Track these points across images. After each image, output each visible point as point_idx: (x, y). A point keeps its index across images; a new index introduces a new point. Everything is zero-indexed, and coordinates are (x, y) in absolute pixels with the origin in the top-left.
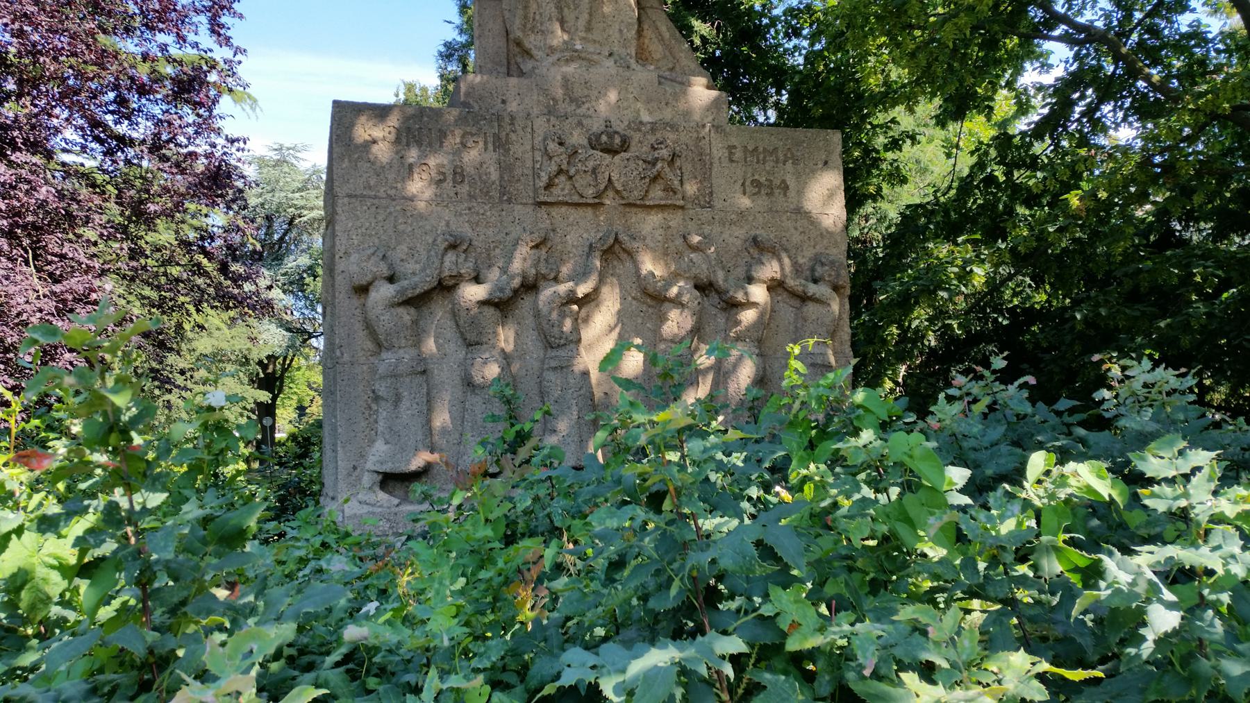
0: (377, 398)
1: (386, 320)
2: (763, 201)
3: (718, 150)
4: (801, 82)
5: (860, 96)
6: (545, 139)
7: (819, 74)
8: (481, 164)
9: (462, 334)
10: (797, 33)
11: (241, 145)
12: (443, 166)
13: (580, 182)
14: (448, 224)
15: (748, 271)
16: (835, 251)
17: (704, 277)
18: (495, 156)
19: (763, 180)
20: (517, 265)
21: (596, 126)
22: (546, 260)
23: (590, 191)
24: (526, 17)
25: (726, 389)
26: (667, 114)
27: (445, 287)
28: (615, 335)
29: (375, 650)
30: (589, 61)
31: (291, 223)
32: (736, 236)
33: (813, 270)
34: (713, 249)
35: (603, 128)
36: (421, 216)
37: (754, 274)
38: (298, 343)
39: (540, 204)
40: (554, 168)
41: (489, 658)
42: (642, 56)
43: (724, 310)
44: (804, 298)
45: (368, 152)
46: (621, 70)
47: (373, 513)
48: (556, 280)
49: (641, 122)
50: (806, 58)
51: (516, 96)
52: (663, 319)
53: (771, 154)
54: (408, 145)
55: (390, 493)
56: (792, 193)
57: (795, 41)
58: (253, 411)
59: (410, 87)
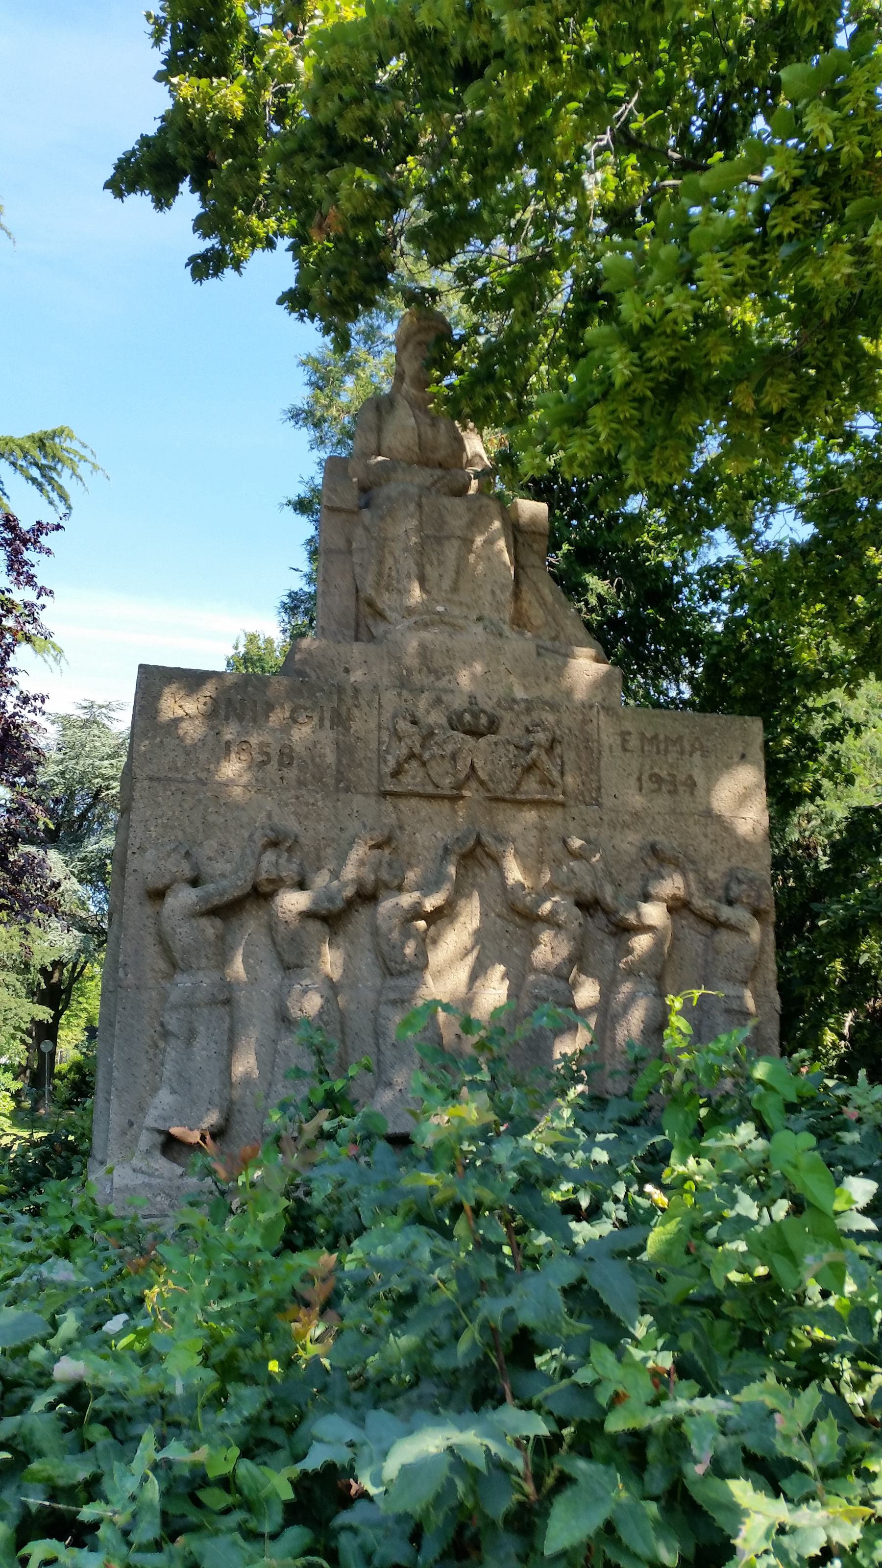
0: (166, 1034)
1: (184, 934)
2: (662, 802)
3: (607, 733)
4: (720, 654)
5: (792, 674)
6: (395, 716)
7: (742, 645)
8: (315, 743)
9: (279, 954)
10: (715, 596)
11: (38, 704)
12: (268, 745)
13: (436, 769)
14: (269, 816)
15: (645, 886)
16: (755, 865)
17: (587, 893)
18: (332, 735)
19: (664, 774)
20: (350, 872)
21: (458, 703)
22: (390, 865)
23: (447, 781)
24: (380, 574)
25: (613, 1040)
26: (547, 691)
27: (261, 894)
28: (470, 959)
29: (99, 1391)
30: (453, 626)
31: (96, 796)
32: (629, 842)
33: (727, 888)
34: (598, 856)
35: (466, 705)
36: (237, 807)
37: (652, 891)
38: (92, 946)
39: (385, 794)
40: (405, 751)
41: (240, 1413)
42: (519, 621)
43: (613, 934)
44: (716, 924)
45: (177, 728)
46: (491, 638)
47: (150, 1186)
48: (400, 889)
49: (514, 701)
50: (726, 626)
51: (361, 667)
52: (534, 942)
53: (674, 743)
54: (227, 718)
55: (174, 1160)
56: (700, 792)
57: (712, 605)
58: (28, 1032)
59: (252, 639)
